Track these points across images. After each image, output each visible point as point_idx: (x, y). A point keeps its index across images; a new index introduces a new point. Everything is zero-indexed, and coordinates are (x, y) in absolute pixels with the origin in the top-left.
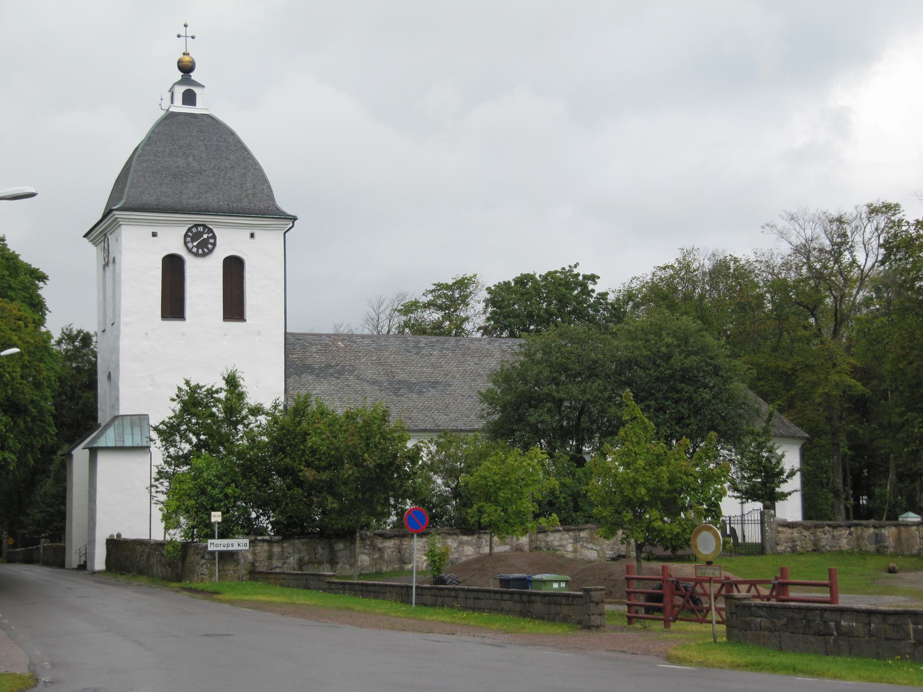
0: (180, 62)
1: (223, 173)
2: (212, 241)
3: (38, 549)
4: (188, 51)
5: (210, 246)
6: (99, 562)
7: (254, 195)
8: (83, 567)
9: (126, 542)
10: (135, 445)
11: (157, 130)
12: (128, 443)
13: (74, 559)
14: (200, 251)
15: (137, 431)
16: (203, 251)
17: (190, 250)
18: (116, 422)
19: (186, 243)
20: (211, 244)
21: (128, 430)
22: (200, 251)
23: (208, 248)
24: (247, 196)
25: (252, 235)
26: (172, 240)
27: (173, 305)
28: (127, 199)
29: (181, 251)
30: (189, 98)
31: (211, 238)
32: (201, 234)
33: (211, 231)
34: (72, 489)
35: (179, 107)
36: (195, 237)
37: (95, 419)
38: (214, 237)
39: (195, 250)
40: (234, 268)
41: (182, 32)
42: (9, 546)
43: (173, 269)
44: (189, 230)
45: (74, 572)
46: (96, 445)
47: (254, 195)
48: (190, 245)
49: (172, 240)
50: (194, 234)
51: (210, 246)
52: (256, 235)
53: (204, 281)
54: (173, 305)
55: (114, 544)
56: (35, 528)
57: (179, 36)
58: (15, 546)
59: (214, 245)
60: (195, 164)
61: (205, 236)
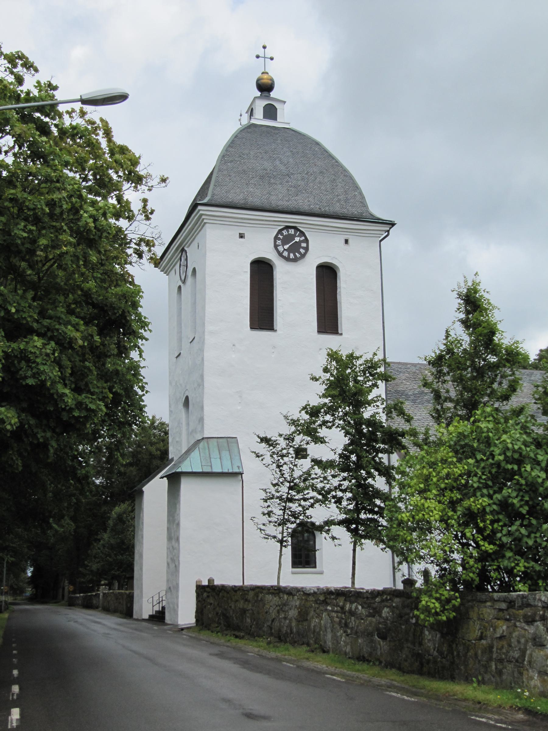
0: (258, 81)
1: (312, 178)
2: (304, 245)
3: (97, 596)
4: (267, 71)
5: (302, 251)
6: (186, 613)
7: (347, 200)
8: (159, 617)
9: (223, 589)
10: (226, 470)
11: (240, 136)
12: (217, 469)
13: (145, 607)
14: (292, 256)
15: (225, 454)
16: (295, 255)
17: (280, 254)
18: (201, 445)
19: (276, 246)
20: (303, 248)
21: (215, 454)
22: (292, 256)
23: (300, 253)
24: (339, 201)
25: (346, 241)
26: (262, 243)
27: (263, 315)
28: (212, 196)
29: (270, 255)
30: (270, 112)
31: (303, 241)
32: (292, 237)
33: (302, 234)
34: (142, 530)
35: (259, 119)
36: (287, 239)
37: (165, 452)
38: (306, 241)
39: (286, 254)
40: (327, 274)
41: (261, 52)
42: (69, 592)
43: (262, 273)
44: (280, 232)
45: (145, 624)
46: (179, 470)
47: (347, 200)
48: (281, 249)
49: (262, 244)
50: (285, 237)
51: (302, 251)
52: (350, 241)
53: (296, 291)
54: (263, 315)
55: (208, 593)
56: (91, 577)
57: (258, 57)
58: (74, 592)
59: (307, 249)
60: (282, 168)
61: (297, 239)
